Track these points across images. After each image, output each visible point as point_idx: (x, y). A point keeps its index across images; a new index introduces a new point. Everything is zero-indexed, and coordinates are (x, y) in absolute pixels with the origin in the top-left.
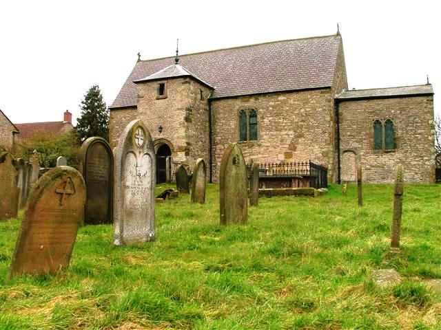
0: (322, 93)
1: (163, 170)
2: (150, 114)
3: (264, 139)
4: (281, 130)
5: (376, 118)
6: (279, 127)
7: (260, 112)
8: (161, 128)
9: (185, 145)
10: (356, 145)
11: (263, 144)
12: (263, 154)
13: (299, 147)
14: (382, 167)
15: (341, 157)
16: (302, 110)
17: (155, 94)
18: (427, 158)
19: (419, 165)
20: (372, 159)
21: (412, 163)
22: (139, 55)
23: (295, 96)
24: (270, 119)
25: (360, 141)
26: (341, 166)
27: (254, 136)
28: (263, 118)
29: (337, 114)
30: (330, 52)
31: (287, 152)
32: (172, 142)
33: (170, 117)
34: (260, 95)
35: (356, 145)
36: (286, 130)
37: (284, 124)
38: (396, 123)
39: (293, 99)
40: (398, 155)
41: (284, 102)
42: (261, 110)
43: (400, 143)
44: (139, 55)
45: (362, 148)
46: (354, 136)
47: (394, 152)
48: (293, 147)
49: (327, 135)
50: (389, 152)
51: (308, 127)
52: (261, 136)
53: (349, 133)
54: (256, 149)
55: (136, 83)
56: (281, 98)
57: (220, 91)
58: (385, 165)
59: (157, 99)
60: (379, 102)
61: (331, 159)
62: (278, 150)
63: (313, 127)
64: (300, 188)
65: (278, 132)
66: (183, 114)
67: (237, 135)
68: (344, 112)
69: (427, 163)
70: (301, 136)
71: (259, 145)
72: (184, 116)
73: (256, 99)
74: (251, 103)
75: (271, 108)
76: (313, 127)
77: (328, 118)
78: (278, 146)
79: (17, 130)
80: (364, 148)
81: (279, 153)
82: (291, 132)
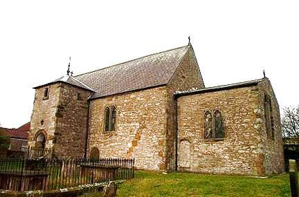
4: (130, 123)
5: (206, 109)
8: (42, 122)
9: (53, 135)
10: (191, 134)
13: (142, 136)
14: (212, 154)
15: (178, 145)
16: (146, 105)
18: (254, 147)
19: (246, 154)
20: (203, 147)
21: (239, 151)
23: (141, 93)
24: (124, 113)
25: (193, 131)
26: (178, 153)
27: (113, 128)
29: (176, 108)
30: (188, 64)
34: (118, 94)
35: (191, 134)
36: (133, 122)
38: (225, 114)
39: (140, 97)
40: (227, 143)
45: (195, 137)
46: (188, 126)
49: (162, 125)
50: (218, 141)
53: (185, 124)
54: (114, 138)
55: (35, 88)
56: (132, 96)
57: (98, 93)
58: (215, 153)
60: (209, 94)
61: (165, 147)
62: (128, 139)
63: (152, 119)
64: (46, 192)
65: (129, 124)
66: (55, 110)
67: (103, 126)
68: (181, 106)
69: (254, 151)
70: (144, 127)
72: (56, 112)
73: (117, 98)
74: (113, 101)
75: (125, 105)
76: (152, 119)
77: (164, 111)
80: (196, 137)
81: (129, 141)
82: (138, 124)
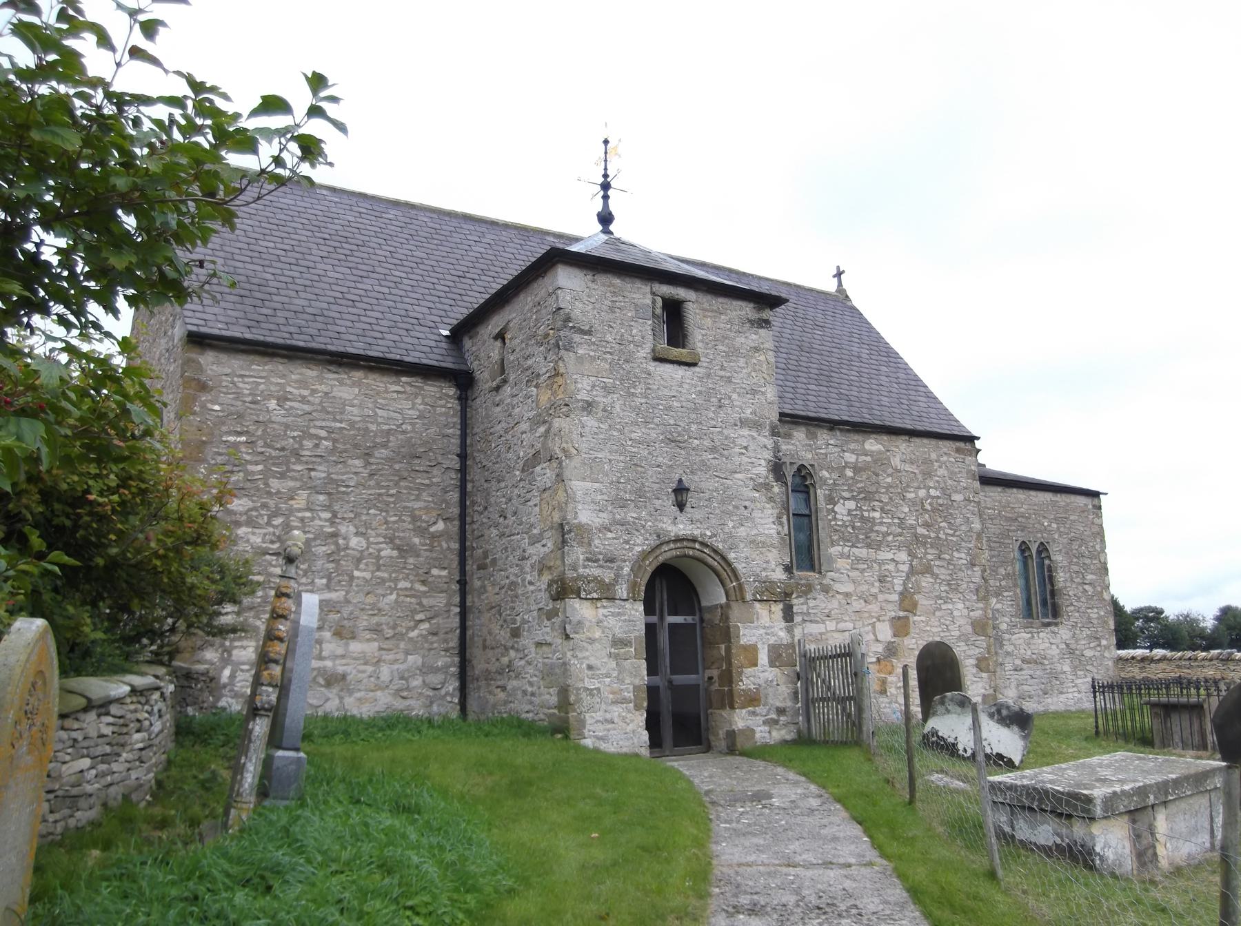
0: (958, 450)
1: (1177, 738)
2: (630, 416)
3: (838, 571)
6: (873, 535)
7: (824, 481)
8: (681, 491)
11: (837, 587)
12: (839, 620)
13: (923, 602)
17: (645, 334)
22: (331, 164)
28: (831, 500)
31: (899, 618)
32: (731, 556)
33: (713, 450)
37: (884, 529)
38: (1053, 548)
40: (1064, 633)
41: (880, 461)
42: (825, 474)
43: (1067, 609)
44: (331, 164)
47: (1056, 624)
48: (908, 602)
51: (937, 544)
52: (831, 560)
56: (873, 444)
59: (659, 359)
62: (874, 608)
71: (826, 590)
75: (849, 473)
78: (875, 596)
79: (137, 309)
82: (903, 556)
